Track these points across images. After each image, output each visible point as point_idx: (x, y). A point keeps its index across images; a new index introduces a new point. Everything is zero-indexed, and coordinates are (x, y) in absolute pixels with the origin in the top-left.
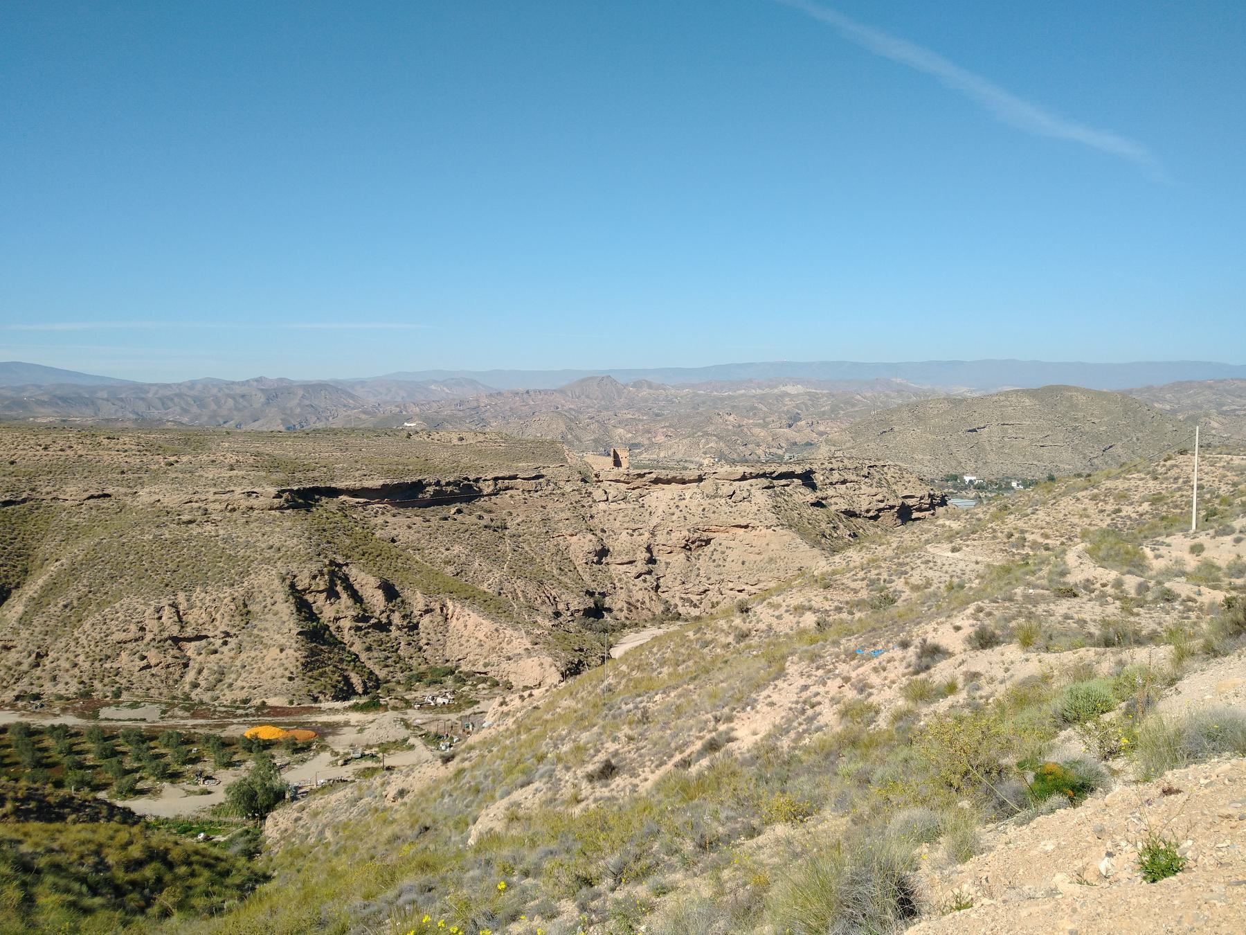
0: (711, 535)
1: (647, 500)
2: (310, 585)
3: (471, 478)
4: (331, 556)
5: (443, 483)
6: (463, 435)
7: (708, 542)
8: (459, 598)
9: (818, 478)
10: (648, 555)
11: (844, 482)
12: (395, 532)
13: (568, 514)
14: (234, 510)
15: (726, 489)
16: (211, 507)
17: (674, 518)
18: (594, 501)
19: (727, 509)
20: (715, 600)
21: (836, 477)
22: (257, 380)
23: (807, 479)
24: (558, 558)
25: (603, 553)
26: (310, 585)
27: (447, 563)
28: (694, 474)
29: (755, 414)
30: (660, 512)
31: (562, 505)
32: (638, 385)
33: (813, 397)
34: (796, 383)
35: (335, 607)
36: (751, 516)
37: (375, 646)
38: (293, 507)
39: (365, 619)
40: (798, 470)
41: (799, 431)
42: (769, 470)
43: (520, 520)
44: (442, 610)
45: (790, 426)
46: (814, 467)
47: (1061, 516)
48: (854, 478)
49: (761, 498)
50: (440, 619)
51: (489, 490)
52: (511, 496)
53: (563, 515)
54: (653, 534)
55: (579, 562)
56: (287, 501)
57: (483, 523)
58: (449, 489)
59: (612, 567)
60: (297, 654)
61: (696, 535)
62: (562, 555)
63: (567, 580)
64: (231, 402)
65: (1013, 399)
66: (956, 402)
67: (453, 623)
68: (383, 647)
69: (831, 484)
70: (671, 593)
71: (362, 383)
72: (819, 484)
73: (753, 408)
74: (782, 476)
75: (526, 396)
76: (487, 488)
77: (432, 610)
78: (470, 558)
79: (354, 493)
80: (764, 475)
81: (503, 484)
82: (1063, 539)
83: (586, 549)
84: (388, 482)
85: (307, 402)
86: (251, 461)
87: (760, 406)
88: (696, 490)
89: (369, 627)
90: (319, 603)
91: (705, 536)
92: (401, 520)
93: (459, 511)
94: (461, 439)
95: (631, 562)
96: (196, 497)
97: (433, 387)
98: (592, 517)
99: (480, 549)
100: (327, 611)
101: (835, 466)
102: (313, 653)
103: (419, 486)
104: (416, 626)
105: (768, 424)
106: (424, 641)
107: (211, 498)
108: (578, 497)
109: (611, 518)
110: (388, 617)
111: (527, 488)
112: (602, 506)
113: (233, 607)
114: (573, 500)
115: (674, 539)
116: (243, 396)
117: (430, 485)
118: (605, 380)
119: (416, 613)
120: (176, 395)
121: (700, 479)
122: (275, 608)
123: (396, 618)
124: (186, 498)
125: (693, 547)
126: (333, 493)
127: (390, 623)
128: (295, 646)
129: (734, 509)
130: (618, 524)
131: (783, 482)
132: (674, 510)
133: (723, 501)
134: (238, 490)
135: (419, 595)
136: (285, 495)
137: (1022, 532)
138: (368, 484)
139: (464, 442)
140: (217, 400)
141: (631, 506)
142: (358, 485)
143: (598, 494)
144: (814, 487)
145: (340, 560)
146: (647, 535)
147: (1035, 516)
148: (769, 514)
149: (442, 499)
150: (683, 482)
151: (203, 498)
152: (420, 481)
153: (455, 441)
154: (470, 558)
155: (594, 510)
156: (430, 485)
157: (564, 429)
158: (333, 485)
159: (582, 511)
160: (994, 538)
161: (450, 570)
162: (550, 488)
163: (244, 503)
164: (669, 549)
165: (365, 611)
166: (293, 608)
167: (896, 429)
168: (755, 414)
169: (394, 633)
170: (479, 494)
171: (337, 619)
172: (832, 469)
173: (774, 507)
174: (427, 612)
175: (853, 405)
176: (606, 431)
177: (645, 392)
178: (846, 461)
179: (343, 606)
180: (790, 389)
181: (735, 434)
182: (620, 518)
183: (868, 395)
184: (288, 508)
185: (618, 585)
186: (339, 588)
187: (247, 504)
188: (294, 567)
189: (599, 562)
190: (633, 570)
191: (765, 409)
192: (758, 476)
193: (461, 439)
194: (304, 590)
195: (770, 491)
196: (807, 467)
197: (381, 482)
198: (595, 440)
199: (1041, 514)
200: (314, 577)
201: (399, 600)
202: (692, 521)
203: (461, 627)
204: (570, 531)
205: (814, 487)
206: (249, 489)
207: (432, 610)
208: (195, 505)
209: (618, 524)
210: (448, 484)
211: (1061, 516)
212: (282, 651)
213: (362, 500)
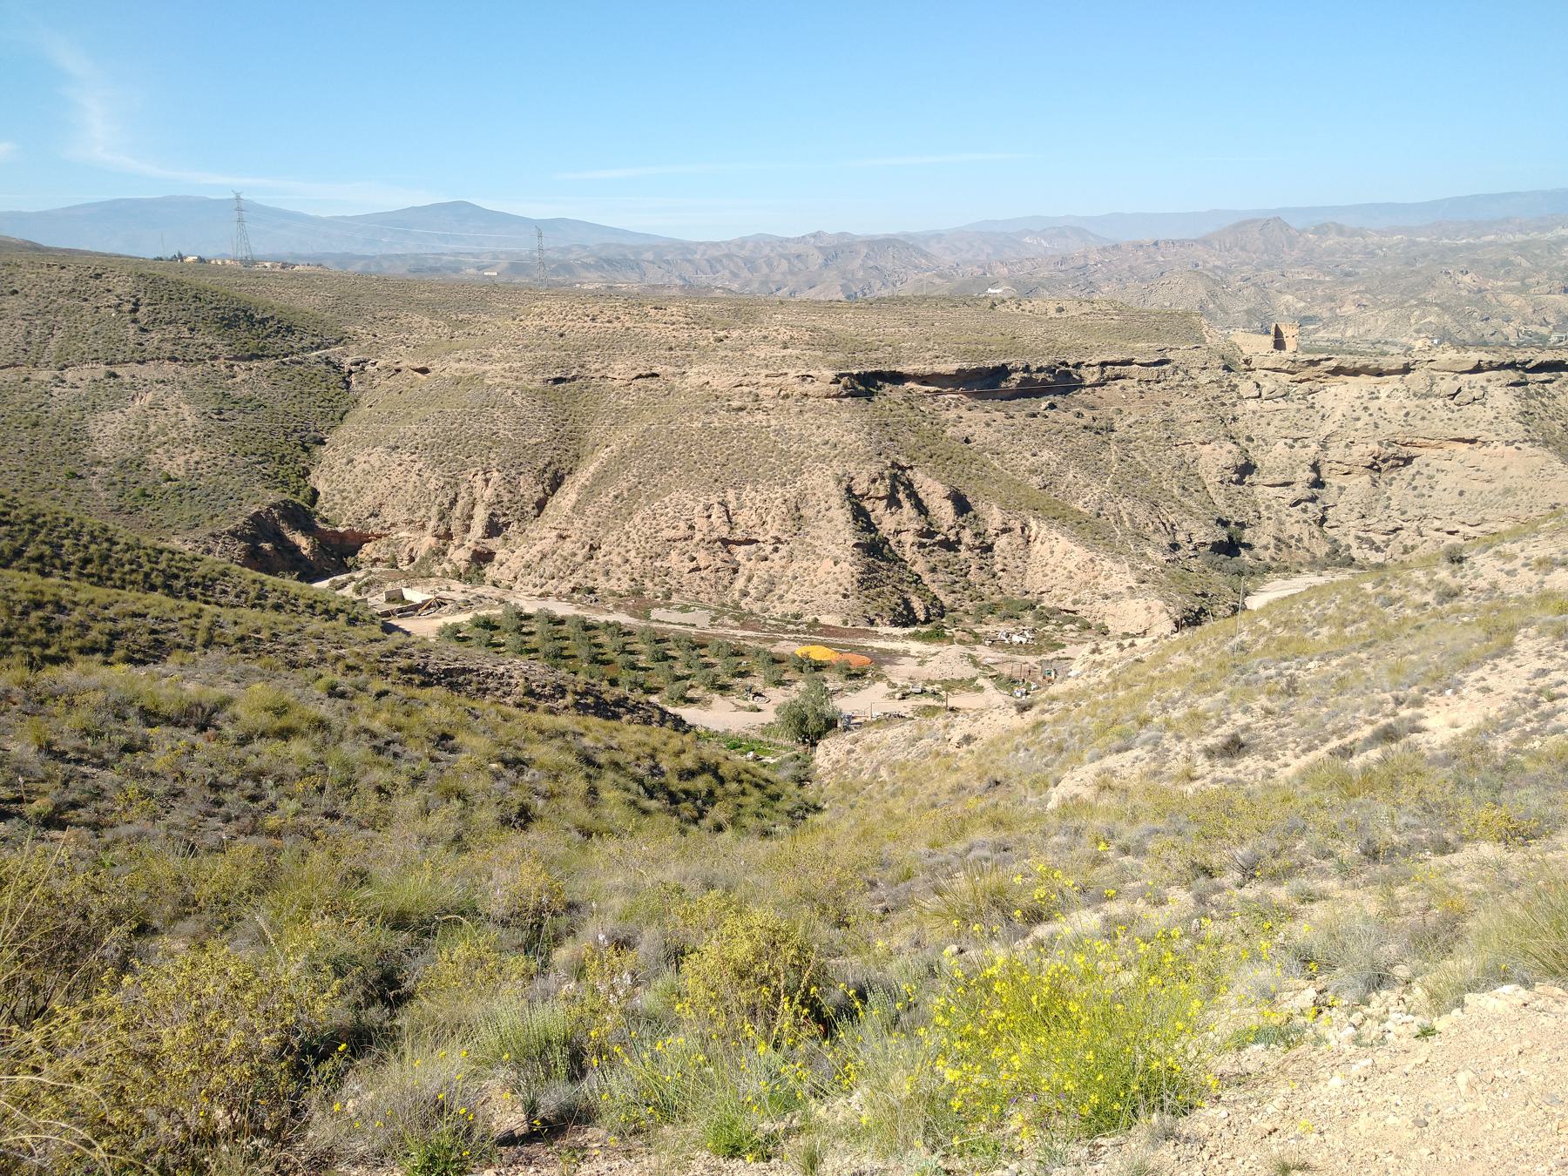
0: (1414, 451)
1: (1319, 398)
3: (1071, 362)
4: (894, 457)
5: (1033, 368)
6: (1064, 304)
7: (1408, 461)
8: (1046, 518)
10: (1314, 475)
13: (1201, 414)
14: (787, 396)
15: (1447, 385)
16: (763, 392)
17: (1359, 424)
18: (1240, 397)
19: (1445, 415)
20: (1409, 543)
24: (1182, 474)
28: (1401, 361)
36: (1482, 425)
37: (940, 567)
39: (930, 534)
43: (1132, 420)
44: (1023, 530)
51: (1094, 379)
52: (1123, 388)
53: (1194, 416)
54: (1324, 446)
55: (1212, 480)
56: (846, 387)
57: (1082, 422)
58: (1041, 376)
60: (852, 569)
61: (1391, 451)
64: (784, 265)
70: (1343, 529)
71: (938, 236)
73: (1506, 263)
75: (1153, 249)
76: (1091, 376)
79: (923, 379)
80: (1512, 366)
81: (1113, 371)
83: (1222, 462)
84: (965, 366)
85: (871, 263)
87: (1519, 259)
90: (878, 512)
91: (1405, 452)
92: (977, 414)
93: (1052, 406)
94: (1060, 310)
95: (1286, 484)
97: (1027, 240)
98: (1234, 419)
102: (870, 570)
103: (1002, 372)
104: (990, 548)
106: (999, 566)
107: (763, 381)
108: (1217, 392)
109: (1263, 421)
111: (1145, 376)
112: (1252, 405)
116: (798, 256)
117: (1016, 370)
118: (1271, 226)
119: (991, 531)
121: (1406, 370)
122: (829, 514)
124: (735, 380)
125: (1384, 466)
126: (898, 378)
128: (850, 559)
129: (1456, 415)
130: (1272, 430)
131: (1544, 376)
132: (1360, 413)
133: (1440, 402)
135: (995, 510)
136: (844, 380)
139: (1064, 315)
141: (1295, 406)
142: (928, 370)
143: (1247, 388)
146: (1314, 447)
148: (1514, 425)
149: (1030, 390)
150: (1379, 373)
153: (1052, 313)
155: (1239, 411)
161: (1035, 481)
162: (1177, 378)
163: (799, 389)
164: (1346, 469)
168: (1508, 273)
169: (964, 554)
170: (1079, 385)
173: (1522, 413)
174: (1004, 531)
176: (1266, 297)
177: (1331, 241)
179: (905, 518)
182: (1276, 422)
185: (1265, 513)
189: (1240, 482)
190: (1289, 495)
191: (1525, 264)
192: (1502, 367)
193: (1060, 310)
195: (1519, 390)
197: (956, 367)
198: (1248, 312)
202: (1387, 430)
204: (1202, 437)
206: (804, 372)
209: (1272, 430)
210: (1040, 370)
212: (836, 563)
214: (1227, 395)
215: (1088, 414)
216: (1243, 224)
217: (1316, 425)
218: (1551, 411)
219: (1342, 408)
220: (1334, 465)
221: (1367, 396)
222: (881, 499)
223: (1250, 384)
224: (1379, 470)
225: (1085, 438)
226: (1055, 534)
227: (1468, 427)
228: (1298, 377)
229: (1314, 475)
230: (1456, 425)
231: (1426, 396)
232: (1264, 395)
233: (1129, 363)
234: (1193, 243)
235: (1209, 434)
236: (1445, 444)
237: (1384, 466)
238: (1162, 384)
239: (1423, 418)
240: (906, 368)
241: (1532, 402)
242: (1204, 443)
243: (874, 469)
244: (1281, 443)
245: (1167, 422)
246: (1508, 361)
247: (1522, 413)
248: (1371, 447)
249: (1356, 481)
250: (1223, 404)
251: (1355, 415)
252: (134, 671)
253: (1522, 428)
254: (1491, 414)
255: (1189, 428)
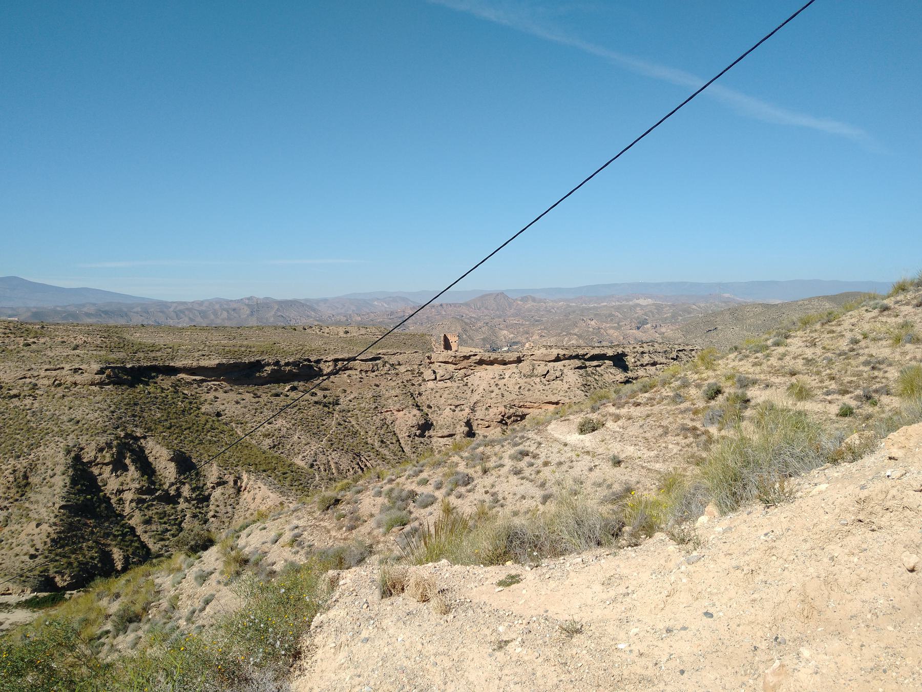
0: (526, 411)
1: (470, 380)
2: (96, 458)
3: (312, 359)
4: (130, 428)
5: (282, 363)
7: (523, 417)
8: (257, 471)
9: (630, 360)
10: (467, 429)
11: (654, 364)
12: (223, 407)
13: (398, 391)
14: (60, 385)
15: (541, 369)
16: (40, 382)
17: (493, 395)
18: (424, 380)
19: (541, 387)
21: (646, 359)
22: (248, 299)
23: (619, 361)
24: (382, 432)
25: (426, 427)
26: (96, 458)
27: (266, 436)
28: (513, 356)
29: (612, 320)
30: (481, 390)
31: (394, 384)
32: (524, 299)
33: (659, 308)
34: (647, 297)
35: (121, 479)
36: (562, 393)
37: (156, 518)
38: (114, 383)
39: (150, 491)
40: (610, 353)
41: (645, 332)
42: (581, 352)
43: (352, 396)
44: (235, 482)
45: (638, 328)
46: (627, 350)
47: (844, 345)
48: (664, 360)
49: (572, 377)
50: (232, 491)
51: (329, 370)
52: (349, 376)
53: (393, 393)
54: (473, 410)
55: (403, 435)
56: (108, 376)
57: (315, 399)
58: (288, 368)
59: (434, 440)
60: (50, 530)
61: (512, 411)
62: (387, 429)
63: (386, 452)
64: (225, 314)
65: (816, 303)
66: (768, 306)
67: (245, 495)
68: (165, 519)
69: (642, 365)
71: (325, 301)
72: (630, 366)
73: (611, 315)
74: (594, 358)
76: (327, 368)
77: (225, 483)
78: (291, 432)
79: (191, 371)
80: (577, 357)
81: (342, 366)
82: (848, 400)
83: (409, 423)
84: (224, 361)
85: (279, 314)
86: (99, 342)
87: (617, 314)
88: (515, 370)
89: (153, 500)
90: (105, 476)
91: (520, 411)
92: (233, 396)
93: (294, 389)
94: (347, 332)
95: (451, 436)
96: (29, 374)
97: (376, 303)
98: (420, 394)
99: (305, 424)
100: (111, 482)
101: (646, 350)
102: (71, 527)
103: (258, 366)
104: (207, 498)
105: (622, 326)
106: (211, 513)
107: (43, 373)
108: (410, 377)
109: (438, 395)
110: (178, 489)
111: (364, 368)
112: (431, 384)
113: (11, 479)
114: (405, 378)
115: (492, 415)
116: (234, 310)
117: (268, 364)
119: (209, 485)
120: (187, 309)
121: (519, 360)
122: (53, 480)
123: (186, 491)
124: (20, 374)
125: (509, 421)
126: (171, 371)
127: (179, 494)
128: (53, 520)
129: (547, 387)
130: (442, 400)
131: (595, 363)
132: (494, 388)
133: (538, 380)
134: (67, 367)
135: (215, 467)
136: (108, 371)
137: (745, 383)
138: (204, 363)
139: (349, 335)
140: (215, 313)
141: (455, 385)
142: (195, 364)
143: (428, 374)
144: (625, 368)
145: (139, 432)
146: (467, 410)
147: (781, 350)
148: (579, 392)
149: (279, 377)
150: (504, 363)
151: (36, 374)
152: (258, 361)
153: (342, 334)
154: (291, 432)
155: (423, 388)
156: (268, 364)
157: (460, 331)
158: (172, 364)
159: (412, 389)
160: (677, 398)
161: (268, 441)
162: (386, 369)
163: (70, 379)
164: (487, 424)
165: (154, 483)
166: (68, 481)
167: (719, 328)
168: (612, 320)
169: (182, 505)
170: (320, 373)
171: (120, 492)
172: (643, 353)
173: (583, 385)
174: (219, 484)
175: (689, 313)
176: (494, 332)
177: (530, 304)
178: (656, 345)
179: (129, 479)
180: (642, 302)
181: (593, 333)
182: (445, 395)
183: (702, 305)
184: (108, 384)
186: (128, 461)
187: (73, 379)
188: (83, 441)
189: (422, 435)
191: (620, 316)
193: (347, 332)
194: (90, 462)
195: (582, 371)
196: (620, 351)
197: (217, 362)
198: (483, 339)
199: (796, 344)
200: (101, 450)
201: (193, 473)
202: (509, 397)
203: (250, 500)
204: (398, 406)
205: (625, 368)
206: (77, 366)
207: (225, 483)
208: (28, 380)
209: (442, 400)
210: (287, 364)
211: (844, 345)
212: (38, 525)
213: (198, 378)
214: (416, 379)
215: (320, 394)
216: (487, 295)
217: (468, 396)
218: (600, 383)
219: (484, 385)
220: (480, 422)
221: (498, 377)
222: (107, 464)
223: (430, 371)
224: (506, 424)
225: (315, 410)
226: (259, 483)
227: (554, 394)
228: (459, 366)
229: (467, 429)
230: (547, 393)
231: (531, 376)
232: (438, 378)
233: (354, 359)
234: (460, 305)
235: (402, 404)
236: (542, 406)
237: (509, 421)
238: (376, 373)
239: (529, 390)
240: (178, 364)
241: (589, 378)
242: (399, 411)
243: (102, 440)
244: (448, 409)
245: (376, 398)
246: (574, 354)
247: (583, 385)
248: (500, 409)
249: (493, 432)
250: (413, 385)
251: (491, 389)
252: (53, 612)
253: (583, 394)
254: (566, 386)
255: (390, 401)
